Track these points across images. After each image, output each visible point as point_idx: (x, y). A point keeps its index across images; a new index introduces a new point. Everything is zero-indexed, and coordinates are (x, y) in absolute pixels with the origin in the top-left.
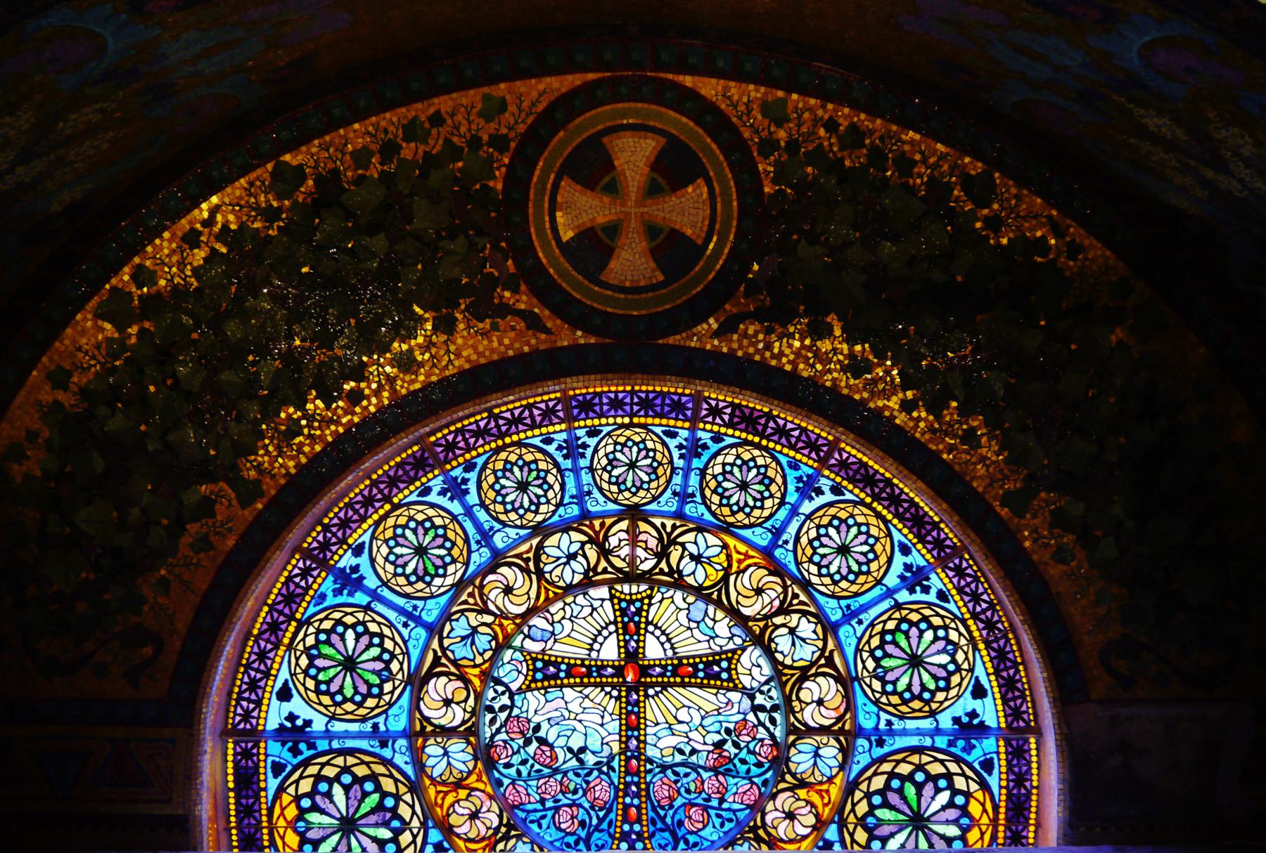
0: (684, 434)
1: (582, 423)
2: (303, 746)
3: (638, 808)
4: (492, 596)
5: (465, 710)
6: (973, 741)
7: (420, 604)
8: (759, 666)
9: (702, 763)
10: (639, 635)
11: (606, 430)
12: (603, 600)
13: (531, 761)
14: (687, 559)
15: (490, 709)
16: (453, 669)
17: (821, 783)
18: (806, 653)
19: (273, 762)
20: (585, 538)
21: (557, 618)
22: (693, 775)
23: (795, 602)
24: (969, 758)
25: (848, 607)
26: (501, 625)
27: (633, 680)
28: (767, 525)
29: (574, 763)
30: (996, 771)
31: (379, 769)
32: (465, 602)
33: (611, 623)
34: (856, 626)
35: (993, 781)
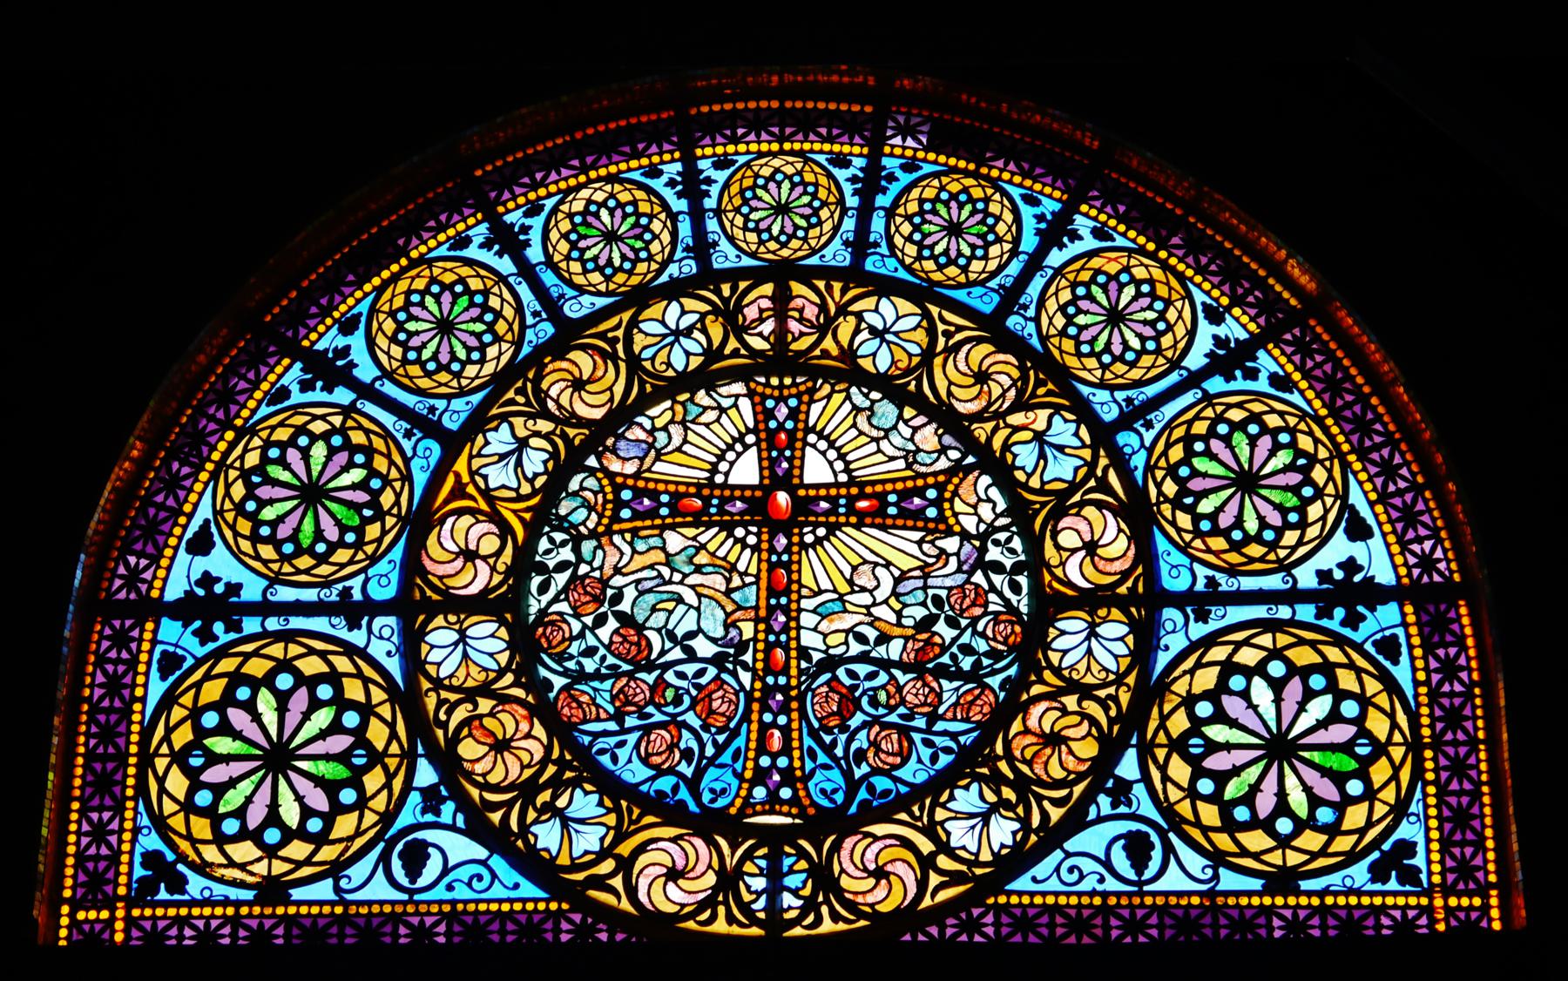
0: (859, 162)
1: (708, 151)
2: (218, 627)
3: (786, 731)
4: (554, 392)
5: (493, 569)
6: (1360, 609)
7: (441, 404)
8: (989, 500)
9: (895, 656)
10: (793, 449)
11: (742, 160)
12: (737, 396)
13: (602, 651)
14: (865, 335)
15: (542, 569)
16: (483, 506)
17: (1105, 685)
18: (1062, 469)
19: (164, 652)
20: (706, 308)
21: (659, 423)
22: (883, 678)
23: (1041, 391)
24: (1357, 637)
25: (1129, 400)
26: (564, 436)
27: (782, 515)
28: (993, 284)
29: (677, 653)
30: (1404, 658)
31: (343, 664)
32: (512, 402)
33: (749, 431)
34: (1142, 430)
35: (1402, 673)
